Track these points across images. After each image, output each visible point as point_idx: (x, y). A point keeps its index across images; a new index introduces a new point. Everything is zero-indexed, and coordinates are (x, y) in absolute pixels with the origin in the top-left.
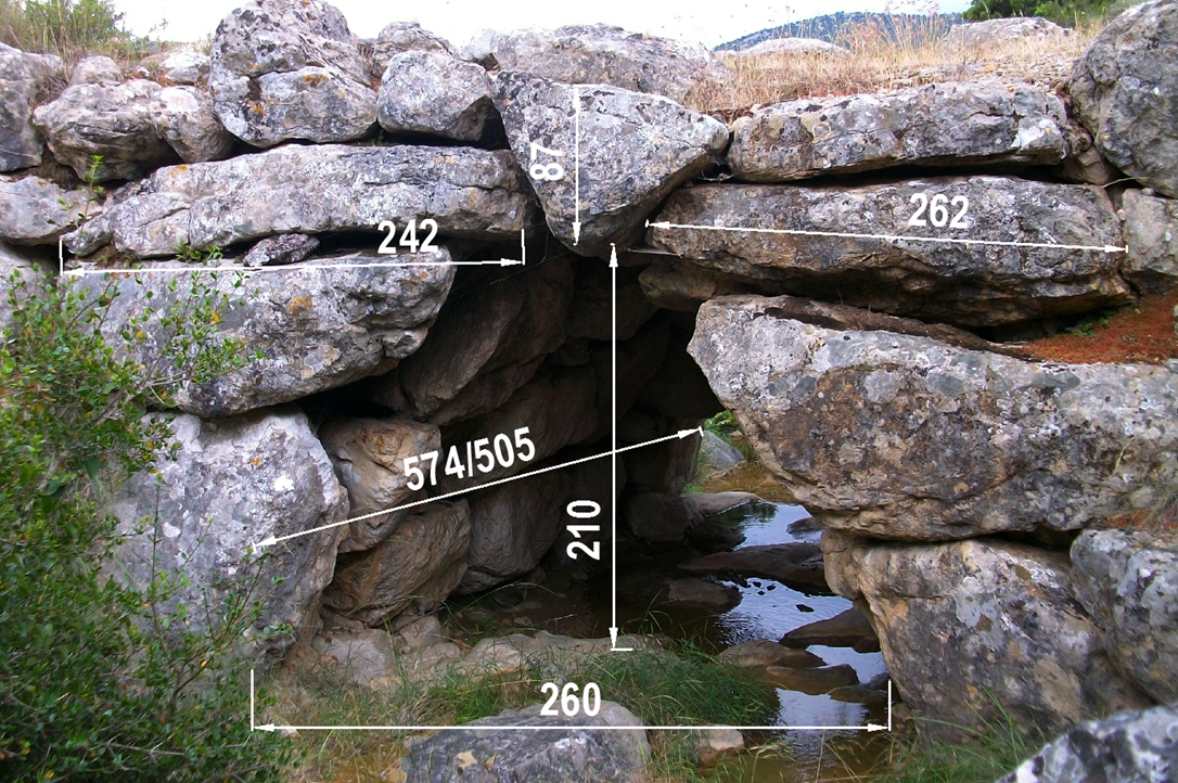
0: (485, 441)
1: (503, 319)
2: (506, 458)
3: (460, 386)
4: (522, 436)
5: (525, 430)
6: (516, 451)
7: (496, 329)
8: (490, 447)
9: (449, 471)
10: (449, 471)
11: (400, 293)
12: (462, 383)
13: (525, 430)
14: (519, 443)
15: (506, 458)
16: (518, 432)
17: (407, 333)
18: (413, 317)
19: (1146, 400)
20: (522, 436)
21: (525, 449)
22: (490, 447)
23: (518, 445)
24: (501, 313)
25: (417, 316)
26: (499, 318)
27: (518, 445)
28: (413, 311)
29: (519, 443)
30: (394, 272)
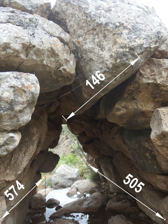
0: (132, 176)
1: (37, 135)
2: (132, 185)
3: (20, 172)
4: (141, 185)
5: (143, 185)
6: (136, 187)
7: (35, 140)
8: (131, 179)
9: (19, 189)
10: (19, 189)
11: (12, 97)
12: (21, 170)
13: (143, 185)
14: (139, 186)
15: (132, 185)
16: (141, 183)
17: (11, 135)
18: (18, 121)
19: (17, 41)
20: (141, 185)
21: (138, 189)
22: (131, 179)
23: (138, 186)
24: (35, 133)
25: (21, 119)
26: (35, 135)
27: (138, 186)
28: (19, 115)
29: (139, 186)
30: (9, 79)
